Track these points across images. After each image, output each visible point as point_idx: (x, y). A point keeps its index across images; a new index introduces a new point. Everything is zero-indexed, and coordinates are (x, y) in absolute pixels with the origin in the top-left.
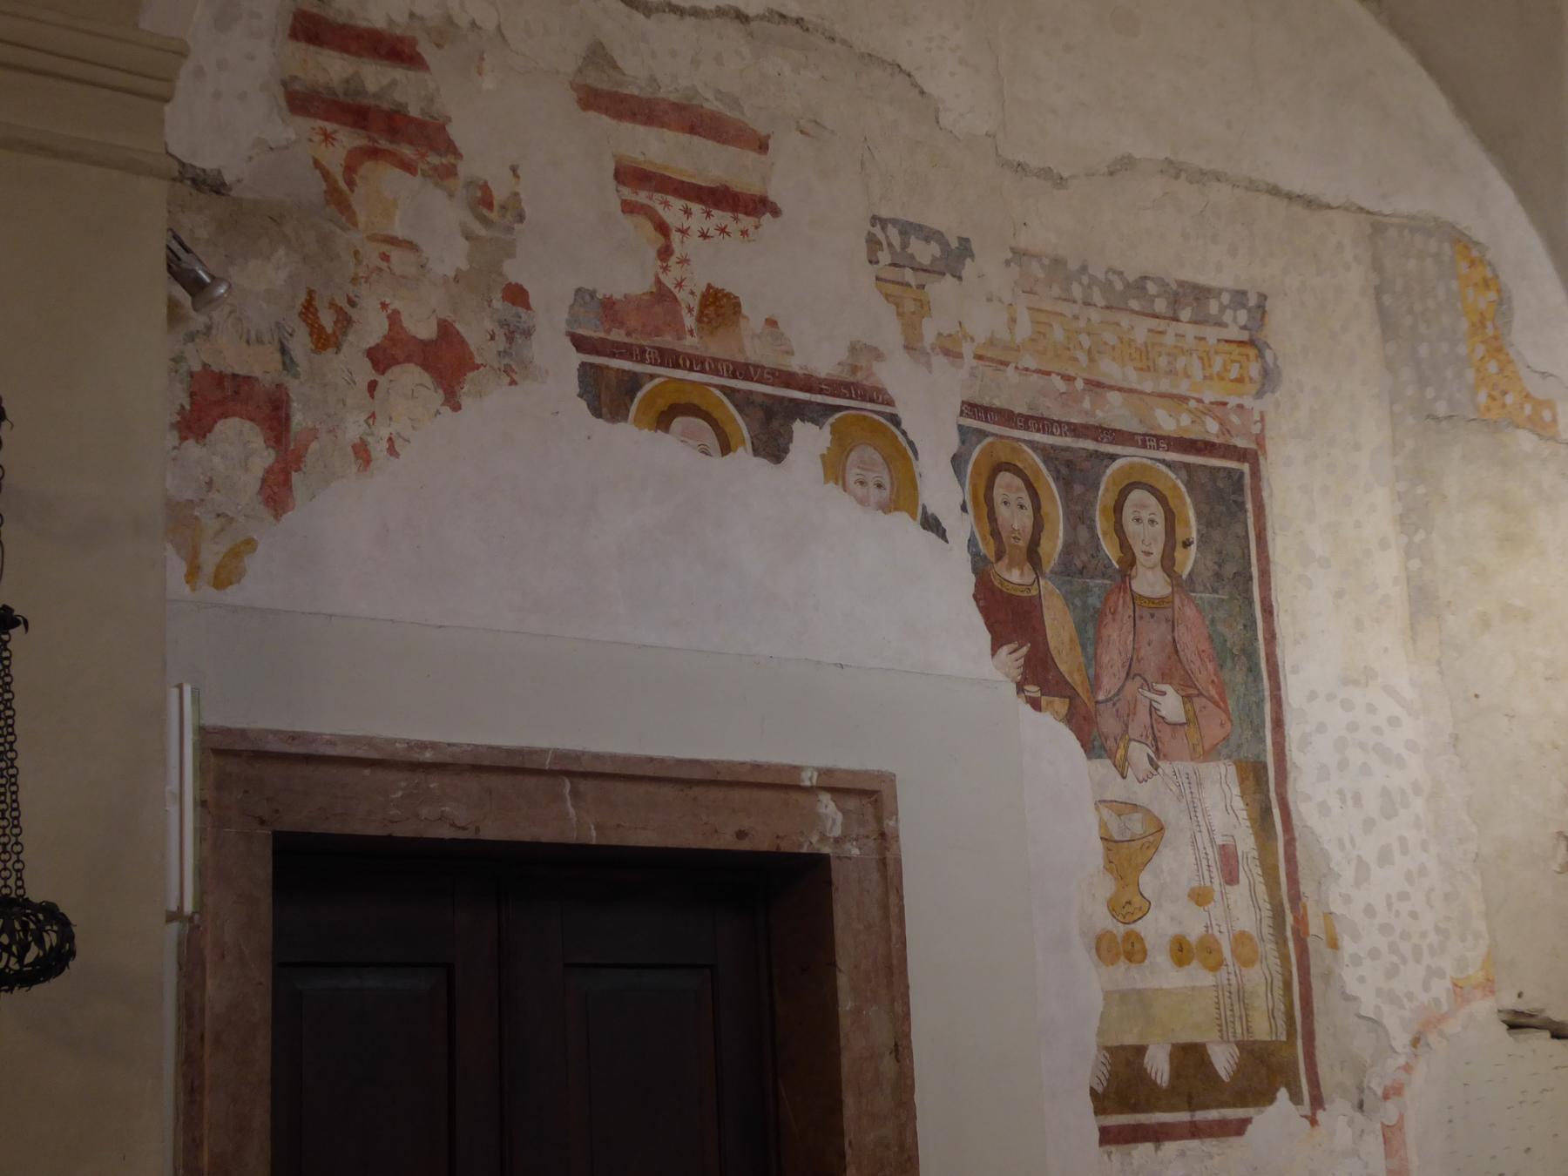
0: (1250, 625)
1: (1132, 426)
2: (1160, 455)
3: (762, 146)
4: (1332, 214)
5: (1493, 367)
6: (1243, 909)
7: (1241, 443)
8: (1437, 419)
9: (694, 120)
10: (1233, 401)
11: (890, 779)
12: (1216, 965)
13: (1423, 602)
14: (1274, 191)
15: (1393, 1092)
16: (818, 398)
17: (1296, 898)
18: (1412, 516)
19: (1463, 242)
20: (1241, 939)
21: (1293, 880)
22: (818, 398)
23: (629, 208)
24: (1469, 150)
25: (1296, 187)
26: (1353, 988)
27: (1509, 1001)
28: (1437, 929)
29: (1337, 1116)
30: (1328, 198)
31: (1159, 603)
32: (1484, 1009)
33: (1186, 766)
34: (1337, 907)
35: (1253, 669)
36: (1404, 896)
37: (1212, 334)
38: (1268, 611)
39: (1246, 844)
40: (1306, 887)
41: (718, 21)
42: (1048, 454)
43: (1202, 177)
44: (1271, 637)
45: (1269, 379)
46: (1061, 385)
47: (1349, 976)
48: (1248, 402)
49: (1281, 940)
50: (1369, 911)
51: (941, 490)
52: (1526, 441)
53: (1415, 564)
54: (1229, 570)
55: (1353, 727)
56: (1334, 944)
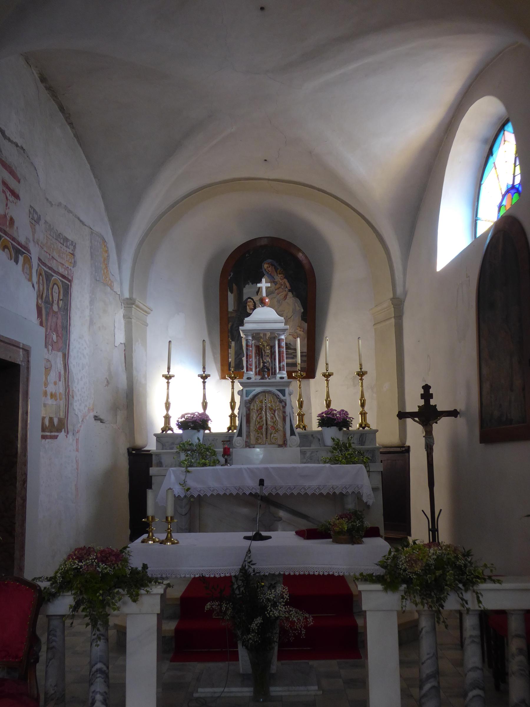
0: (67, 322)
1: (55, 269)
2: (59, 277)
3: (19, 182)
4: (86, 227)
5: (105, 271)
6: (61, 388)
7: (70, 278)
8: (96, 280)
9: (12, 173)
10: (70, 268)
11: (30, 348)
12: (56, 400)
13: (92, 322)
14: (79, 219)
15: (78, 432)
16: (22, 250)
17: (68, 386)
18: (92, 302)
19: (104, 241)
20: (60, 394)
21: (68, 382)
22: (22, 250)
23: (4, 192)
24: (106, 219)
25: (81, 219)
26: (75, 408)
27: (96, 414)
28: (87, 396)
29: (70, 435)
30: (86, 223)
31: (56, 313)
32: (92, 414)
33: (56, 352)
34: (74, 389)
35: (67, 332)
36: (83, 388)
37: (68, 250)
38: (70, 318)
39: (62, 372)
40: (70, 384)
41: (14, 145)
42: (45, 272)
43: (70, 212)
44: (70, 325)
45: (75, 264)
46: (48, 256)
47: (75, 404)
48: (71, 268)
49: (66, 395)
50: (78, 390)
51: (35, 279)
52: (109, 289)
53: (91, 313)
54: (66, 308)
55: (80, 348)
56: (73, 397)
